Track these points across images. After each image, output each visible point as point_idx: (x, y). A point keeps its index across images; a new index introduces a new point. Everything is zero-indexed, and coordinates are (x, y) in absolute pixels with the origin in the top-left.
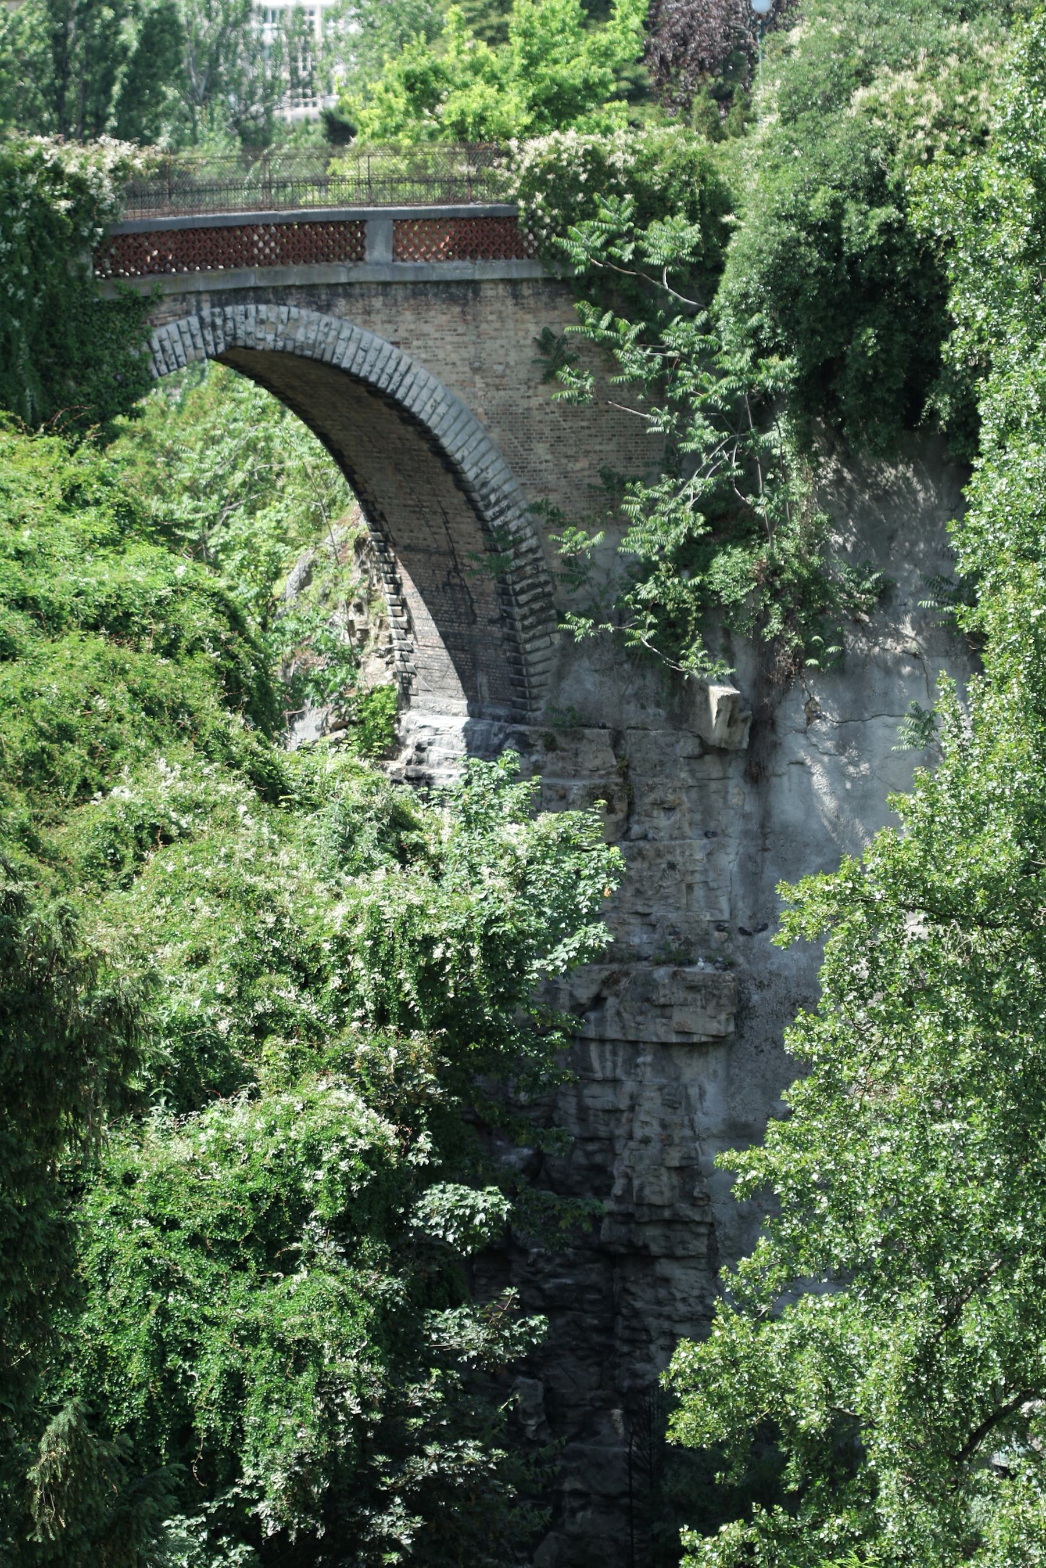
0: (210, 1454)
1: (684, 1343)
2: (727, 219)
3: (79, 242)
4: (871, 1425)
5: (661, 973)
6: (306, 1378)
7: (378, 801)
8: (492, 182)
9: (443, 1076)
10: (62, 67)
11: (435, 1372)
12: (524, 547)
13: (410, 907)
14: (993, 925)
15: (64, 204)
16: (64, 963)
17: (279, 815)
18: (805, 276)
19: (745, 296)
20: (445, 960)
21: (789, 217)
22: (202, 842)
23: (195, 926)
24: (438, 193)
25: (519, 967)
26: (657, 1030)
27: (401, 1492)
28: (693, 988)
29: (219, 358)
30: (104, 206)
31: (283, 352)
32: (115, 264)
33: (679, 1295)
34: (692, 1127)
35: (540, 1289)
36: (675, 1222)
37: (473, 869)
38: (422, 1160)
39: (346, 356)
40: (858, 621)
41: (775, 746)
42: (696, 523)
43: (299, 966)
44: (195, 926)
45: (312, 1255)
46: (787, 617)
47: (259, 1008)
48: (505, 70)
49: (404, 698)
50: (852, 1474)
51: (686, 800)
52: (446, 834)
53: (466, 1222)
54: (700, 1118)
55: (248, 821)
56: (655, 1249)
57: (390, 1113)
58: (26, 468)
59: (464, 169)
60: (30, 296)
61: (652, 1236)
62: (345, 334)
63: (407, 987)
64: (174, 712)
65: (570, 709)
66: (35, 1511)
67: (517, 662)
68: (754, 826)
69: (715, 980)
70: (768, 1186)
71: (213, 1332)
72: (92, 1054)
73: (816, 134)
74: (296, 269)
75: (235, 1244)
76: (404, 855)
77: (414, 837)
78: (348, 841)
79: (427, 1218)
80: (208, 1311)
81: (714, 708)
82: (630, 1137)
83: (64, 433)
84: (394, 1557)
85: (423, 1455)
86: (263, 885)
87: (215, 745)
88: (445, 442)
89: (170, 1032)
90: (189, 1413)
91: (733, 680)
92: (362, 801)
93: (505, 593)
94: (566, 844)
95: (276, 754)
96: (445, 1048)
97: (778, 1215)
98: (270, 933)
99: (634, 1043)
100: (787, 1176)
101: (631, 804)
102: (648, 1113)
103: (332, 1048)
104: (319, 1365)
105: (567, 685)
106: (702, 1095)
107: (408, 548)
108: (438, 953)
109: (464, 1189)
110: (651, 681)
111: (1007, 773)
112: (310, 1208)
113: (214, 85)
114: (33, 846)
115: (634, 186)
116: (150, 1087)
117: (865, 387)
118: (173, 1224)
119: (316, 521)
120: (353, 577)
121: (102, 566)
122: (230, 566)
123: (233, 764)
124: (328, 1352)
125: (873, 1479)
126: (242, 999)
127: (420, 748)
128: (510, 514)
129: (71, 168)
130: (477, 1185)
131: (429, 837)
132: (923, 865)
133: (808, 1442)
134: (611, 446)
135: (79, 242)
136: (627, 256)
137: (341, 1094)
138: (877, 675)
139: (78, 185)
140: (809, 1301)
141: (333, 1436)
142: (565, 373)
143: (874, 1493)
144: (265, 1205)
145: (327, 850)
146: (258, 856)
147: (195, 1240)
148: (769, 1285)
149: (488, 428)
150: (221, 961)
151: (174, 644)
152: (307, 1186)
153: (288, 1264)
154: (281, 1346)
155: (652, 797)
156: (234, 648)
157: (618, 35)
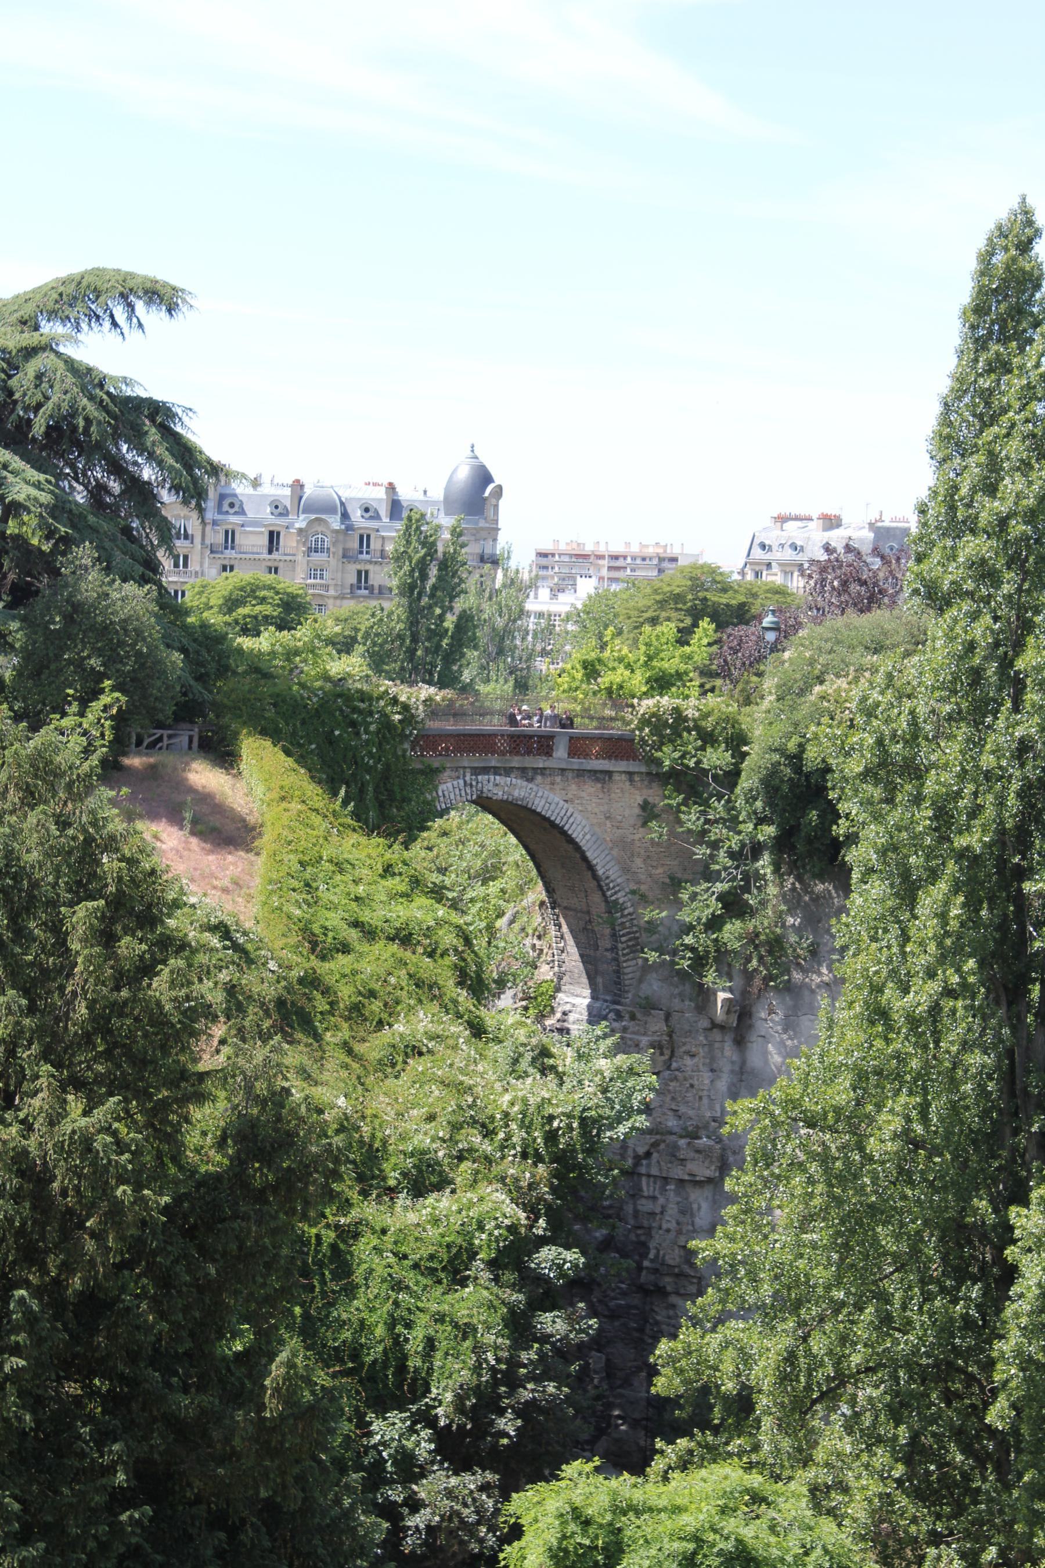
0: (414, 1380)
1: (664, 1340)
2: (745, 749)
3: (404, 737)
4: (760, 1391)
5: (682, 1142)
6: (468, 1343)
7: (534, 1041)
8: (623, 719)
9: (553, 1190)
10: (415, 639)
11: (536, 1345)
12: (626, 912)
13: (543, 1099)
14: (837, 1132)
15: (397, 717)
16: (305, 1123)
17: (481, 1045)
18: (782, 781)
19: (751, 790)
20: (559, 1128)
21: (776, 750)
22: (438, 1057)
23: (431, 1100)
24: (595, 723)
25: (598, 1135)
26: (678, 1173)
27: (512, 1407)
28: (698, 1151)
29: (473, 802)
30: (419, 719)
31: (507, 801)
32: (422, 750)
34: (693, 1224)
36: (681, 1275)
37: (580, 1082)
38: (541, 1232)
39: (539, 806)
40: (799, 964)
41: (750, 1027)
42: (715, 907)
43: (483, 1125)
44: (431, 1100)
45: (476, 1278)
46: (761, 959)
47: (460, 1146)
48: (635, 662)
49: (558, 989)
50: (747, 1417)
51: (701, 1052)
52: (568, 1061)
53: (560, 1267)
54: (697, 1220)
55: (464, 1047)
56: (669, 1289)
57: (525, 1207)
58: (365, 854)
59: (608, 712)
60: (376, 764)
61: (668, 1282)
62: (540, 794)
63: (539, 1140)
64: (430, 987)
65: (647, 998)
66: (267, 1400)
67: (618, 972)
68: (737, 1068)
69: (710, 1148)
70: (716, 1260)
71: (421, 1315)
72: (317, 1171)
73: (793, 708)
74: (516, 758)
75: (436, 1270)
76: (544, 1071)
77: (551, 1061)
78: (516, 1061)
79: (538, 1264)
80: (419, 1304)
81: (719, 1005)
82: (660, 1228)
83: (386, 837)
84: (505, 1441)
85: (525, 1388)
86: (468, 1081)
87: (450, 1005)
88: (588, 854)
89: (412, 1155)
90: (405, 1357)
91: (731, 990)
92: (525, 1041)
93: (614, 936)
94: (631, 1072)
95: (483, 1012)
96: (555, 1174)
97: (719, 1276)
98: (470, 1107)
99: (665, 1178)
100: (725, 1256)
101: (673, 1052)
103: (496, 1170)
104: (475, 1337)
105: (644, 986)
106: (699, 1208)
107: (566, 908)
108: (555, 1124)
109: (561, 1250)
110: (688, 988)
111: (849, 1053)
112: (477, 1253)
113: (501, 652)
114: (350, 1052)
115: (697, 728)
116: (399, 1183)
117: (810, 841)
118: (405, 1257)
119: (521, 890)
120: (537, 920)
121: (400, 907)
122: (474, 910)
123: (459, 1016)
124: (480, 1331)
125: (758, 1421)
126: (452, 1140)
127: (565, 1014)
128: (619, 895)
129: (403, 698)
130: (568, 1248)
131: (559, 1062)
132: (802, 1097)
133: (725, 1398)
134: (676, 863)
135: (404, 737)
136: (692, 764)
137: (498, 1194)
138: (806, 993)
139: (406, 707)
140: (733, 1323)
141: (480, 1375)
142: (653, 824)
143: (759, 1428)
144: (454, 1250)
145: (504, 1066)
146: (467, 1065)
147: (416, 1266)
148: (712, 1313)
149: (611, 849)
150: (442, 1120)
151: (434, 951)
152: (477, 1242)
153: (463, 1283)
154: (456, 1326)
155: (684, 1049)
156: (465, 955)
157: (696, 649)
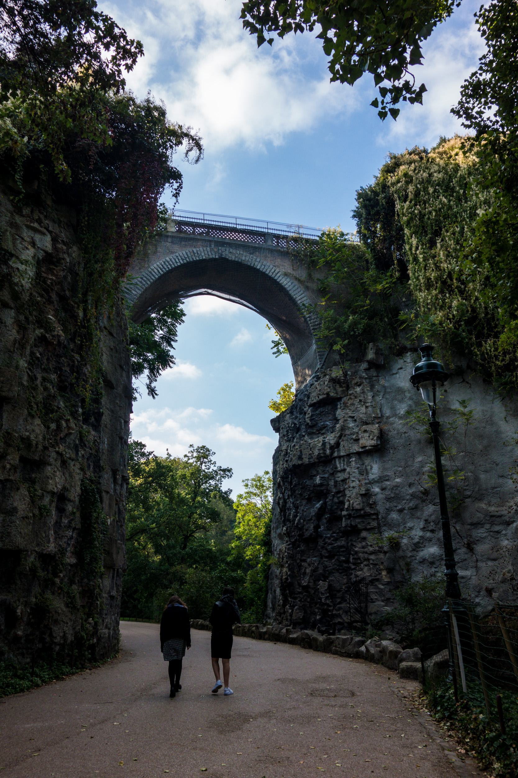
33: (369, 544)
35: (326, 549)
62: (258, 260)
102: (354, 477)
